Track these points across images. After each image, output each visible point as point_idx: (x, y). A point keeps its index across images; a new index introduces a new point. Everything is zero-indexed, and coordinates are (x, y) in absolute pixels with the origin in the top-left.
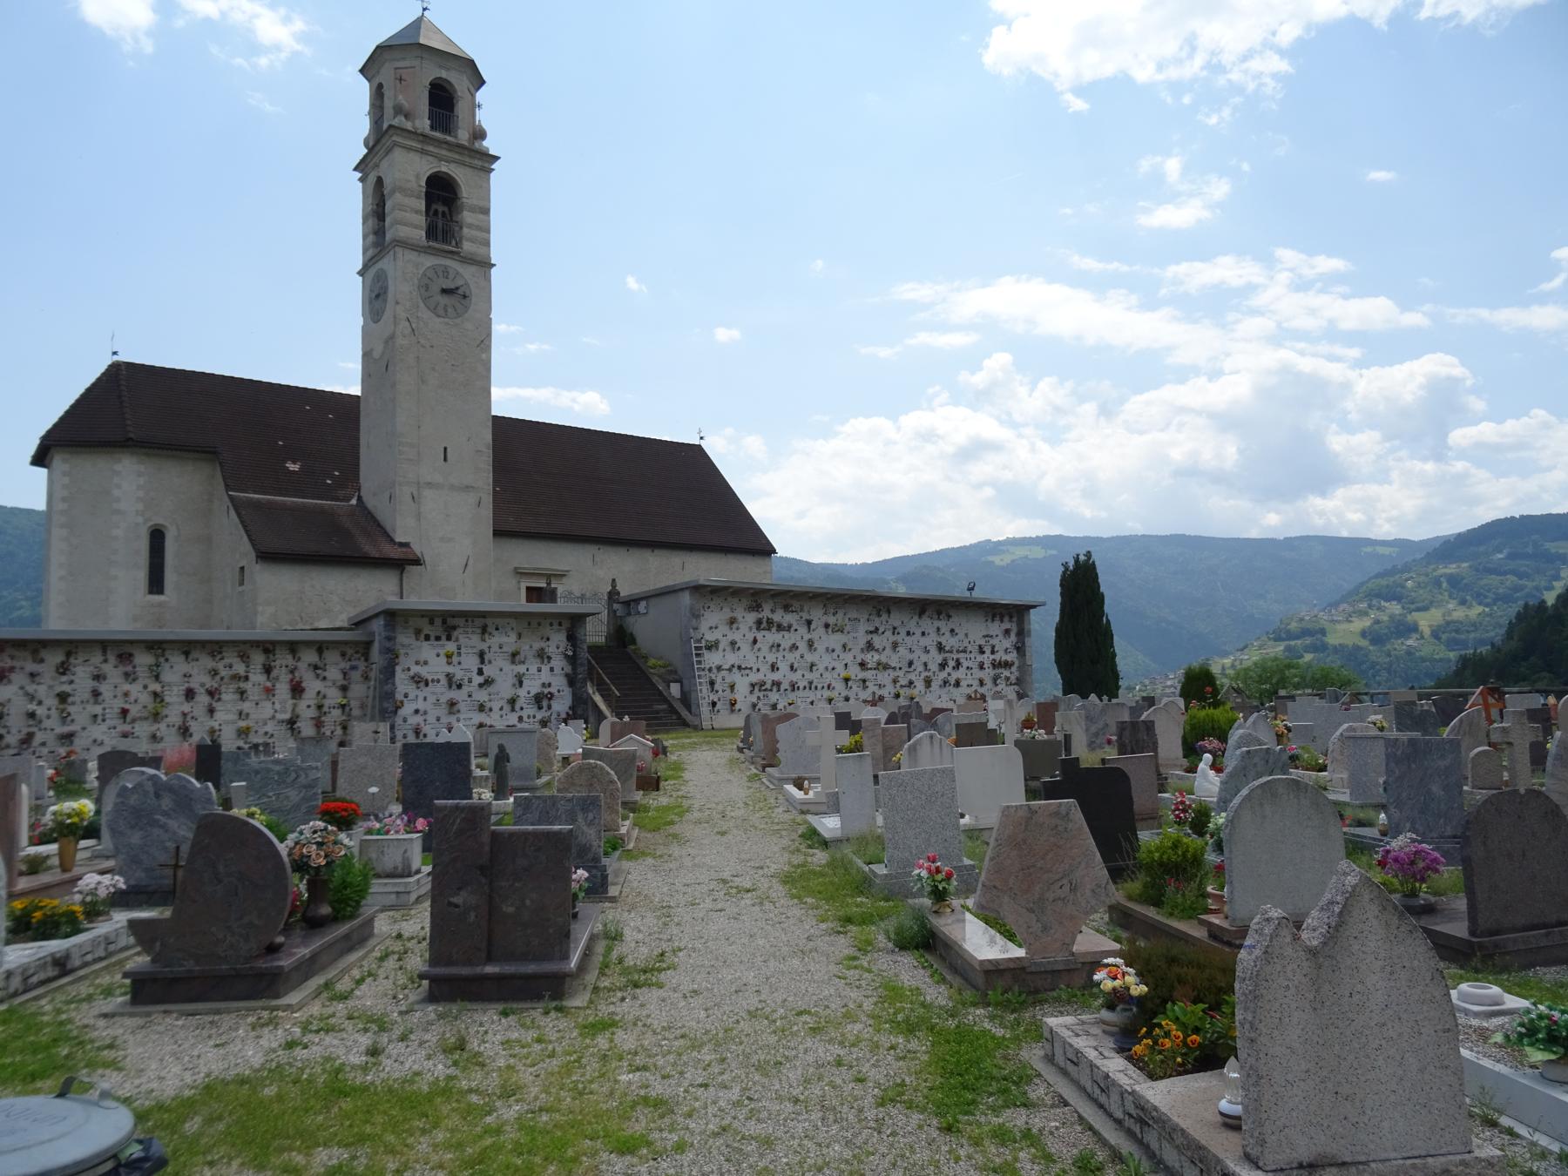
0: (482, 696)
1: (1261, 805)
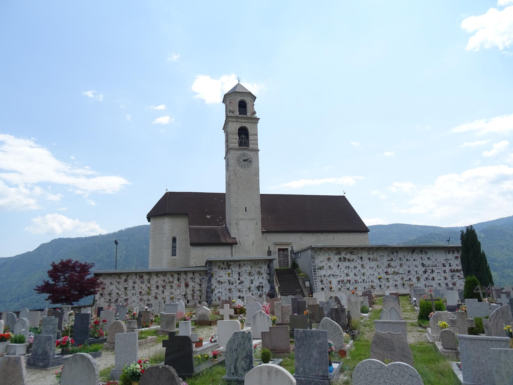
0: (239, 287)
1: (72, 364)
